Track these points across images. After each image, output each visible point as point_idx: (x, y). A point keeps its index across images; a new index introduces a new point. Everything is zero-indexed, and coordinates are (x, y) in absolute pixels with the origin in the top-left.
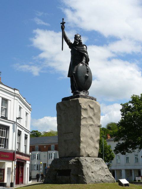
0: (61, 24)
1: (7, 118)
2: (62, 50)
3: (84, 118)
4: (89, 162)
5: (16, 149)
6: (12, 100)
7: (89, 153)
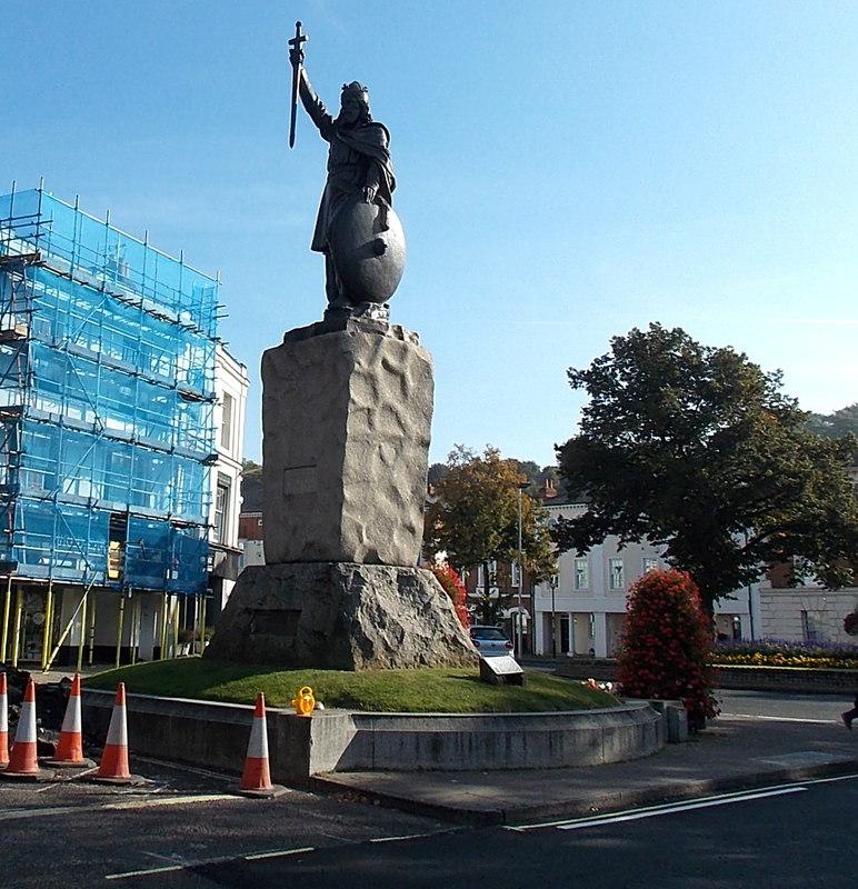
0: (290, 43)
2: (292, 145)
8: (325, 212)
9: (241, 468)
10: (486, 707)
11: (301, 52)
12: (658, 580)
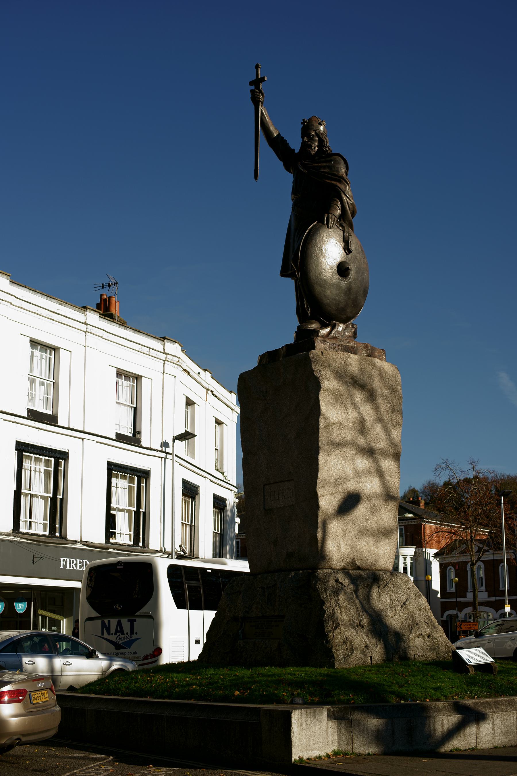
0: (251, 83)
2: (256, 178)
8: (291, 241)
9: (236, 490)
10: (307, 715)
11: (260, 91)
12: (335, 377)
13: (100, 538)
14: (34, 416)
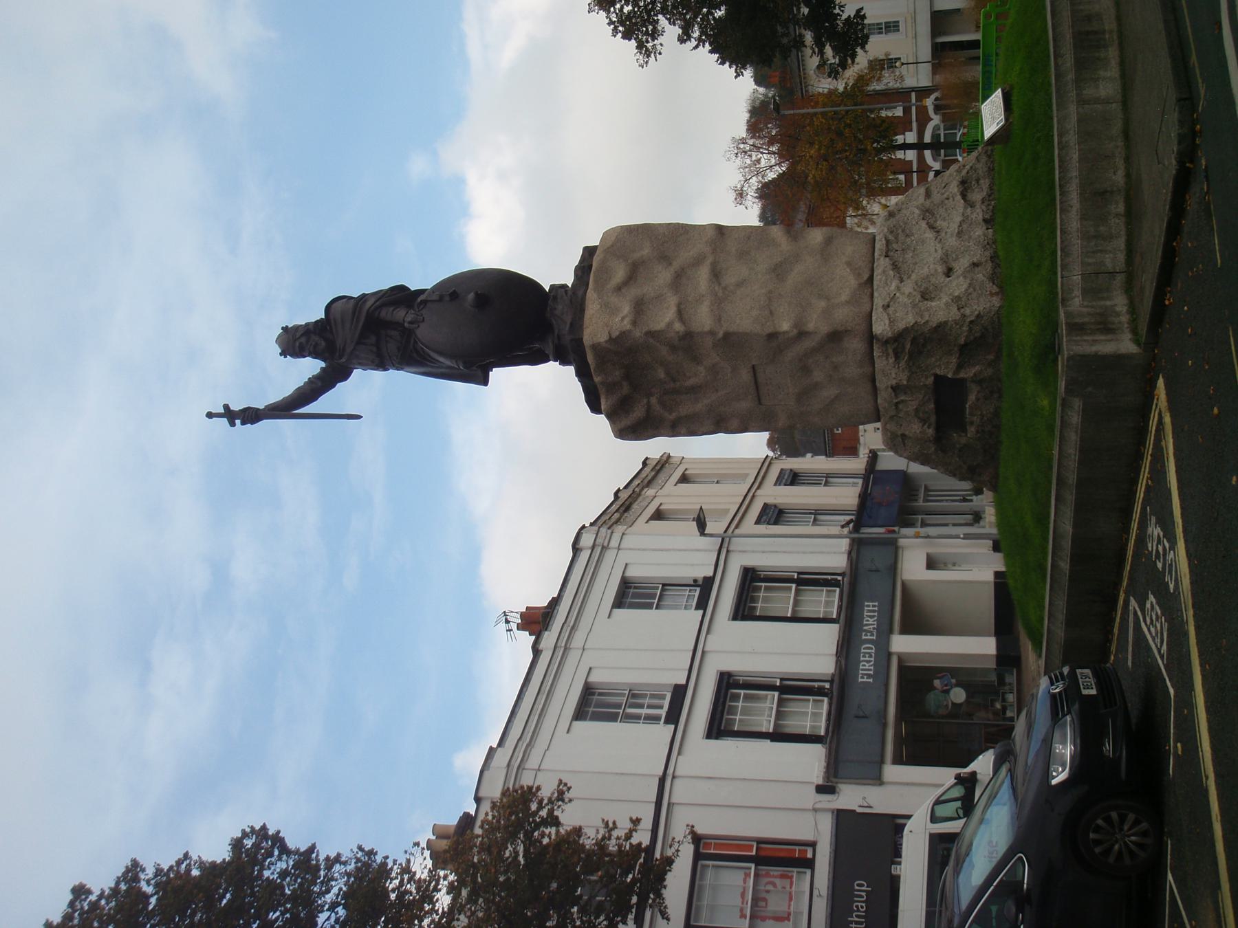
0: (233, 424)
1: (705, 578)
2: (358, 417)
3: (680, 313)
4: (898, 288)
5: (846, 530)
6: (624, 557)
7: (853, 282)
13: (835, 628)
14: (673, 717)
